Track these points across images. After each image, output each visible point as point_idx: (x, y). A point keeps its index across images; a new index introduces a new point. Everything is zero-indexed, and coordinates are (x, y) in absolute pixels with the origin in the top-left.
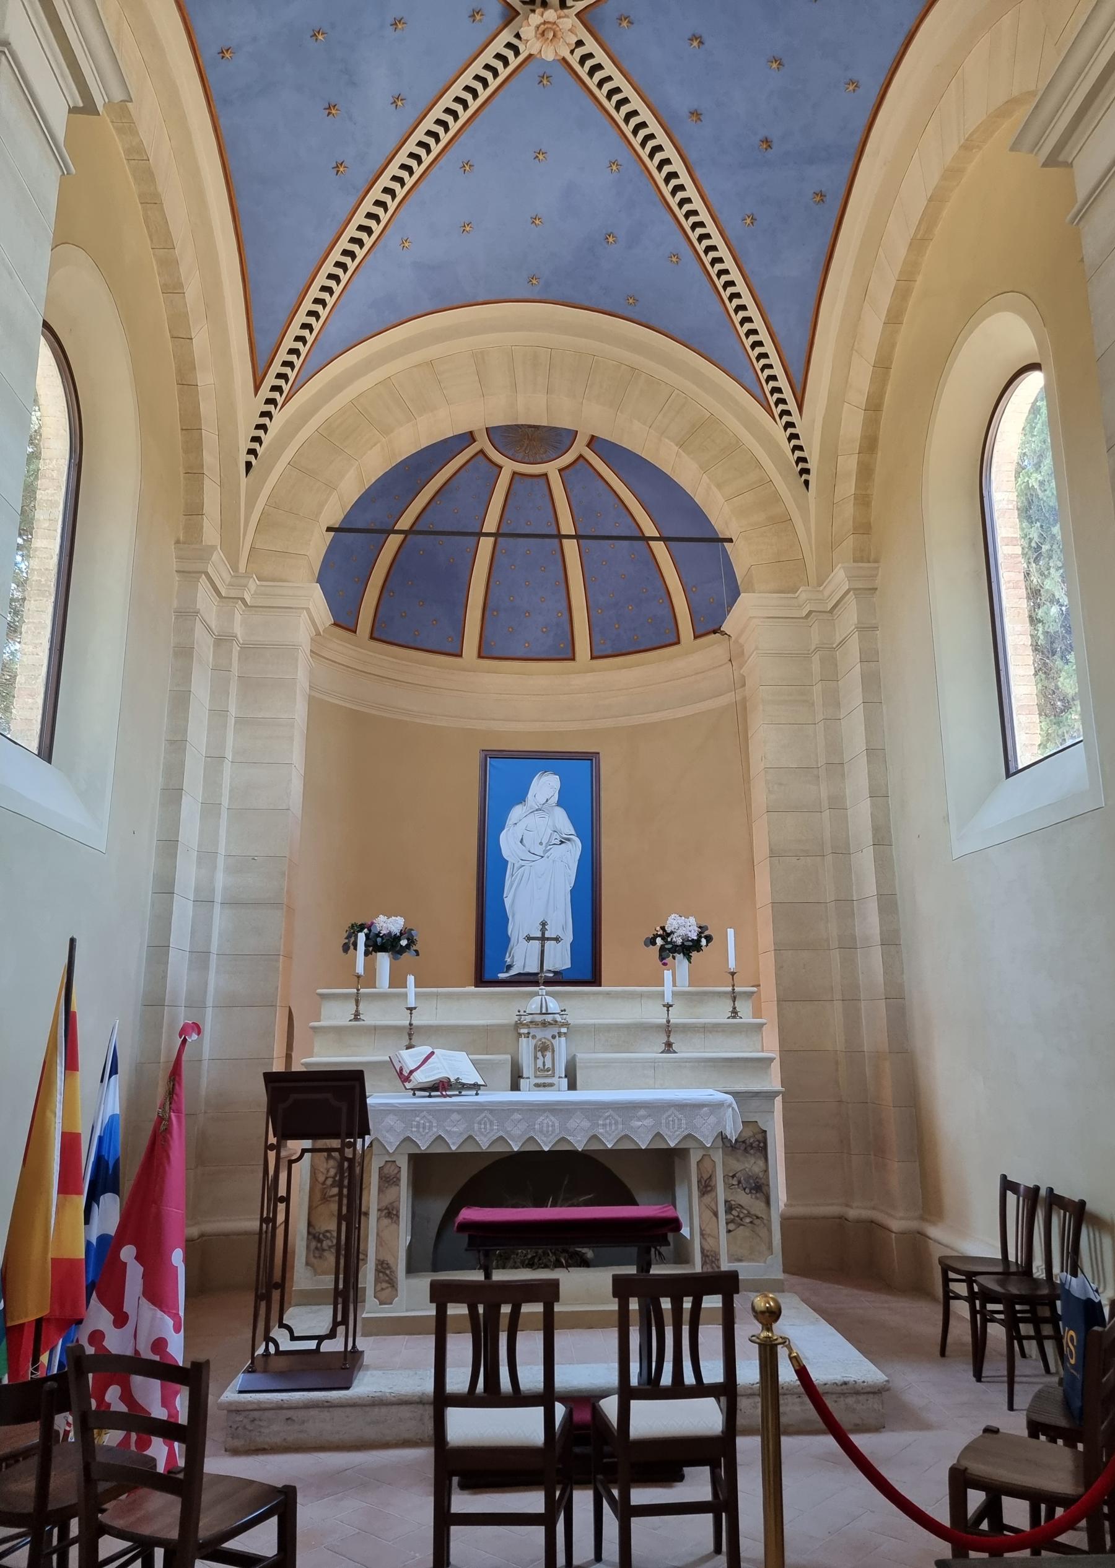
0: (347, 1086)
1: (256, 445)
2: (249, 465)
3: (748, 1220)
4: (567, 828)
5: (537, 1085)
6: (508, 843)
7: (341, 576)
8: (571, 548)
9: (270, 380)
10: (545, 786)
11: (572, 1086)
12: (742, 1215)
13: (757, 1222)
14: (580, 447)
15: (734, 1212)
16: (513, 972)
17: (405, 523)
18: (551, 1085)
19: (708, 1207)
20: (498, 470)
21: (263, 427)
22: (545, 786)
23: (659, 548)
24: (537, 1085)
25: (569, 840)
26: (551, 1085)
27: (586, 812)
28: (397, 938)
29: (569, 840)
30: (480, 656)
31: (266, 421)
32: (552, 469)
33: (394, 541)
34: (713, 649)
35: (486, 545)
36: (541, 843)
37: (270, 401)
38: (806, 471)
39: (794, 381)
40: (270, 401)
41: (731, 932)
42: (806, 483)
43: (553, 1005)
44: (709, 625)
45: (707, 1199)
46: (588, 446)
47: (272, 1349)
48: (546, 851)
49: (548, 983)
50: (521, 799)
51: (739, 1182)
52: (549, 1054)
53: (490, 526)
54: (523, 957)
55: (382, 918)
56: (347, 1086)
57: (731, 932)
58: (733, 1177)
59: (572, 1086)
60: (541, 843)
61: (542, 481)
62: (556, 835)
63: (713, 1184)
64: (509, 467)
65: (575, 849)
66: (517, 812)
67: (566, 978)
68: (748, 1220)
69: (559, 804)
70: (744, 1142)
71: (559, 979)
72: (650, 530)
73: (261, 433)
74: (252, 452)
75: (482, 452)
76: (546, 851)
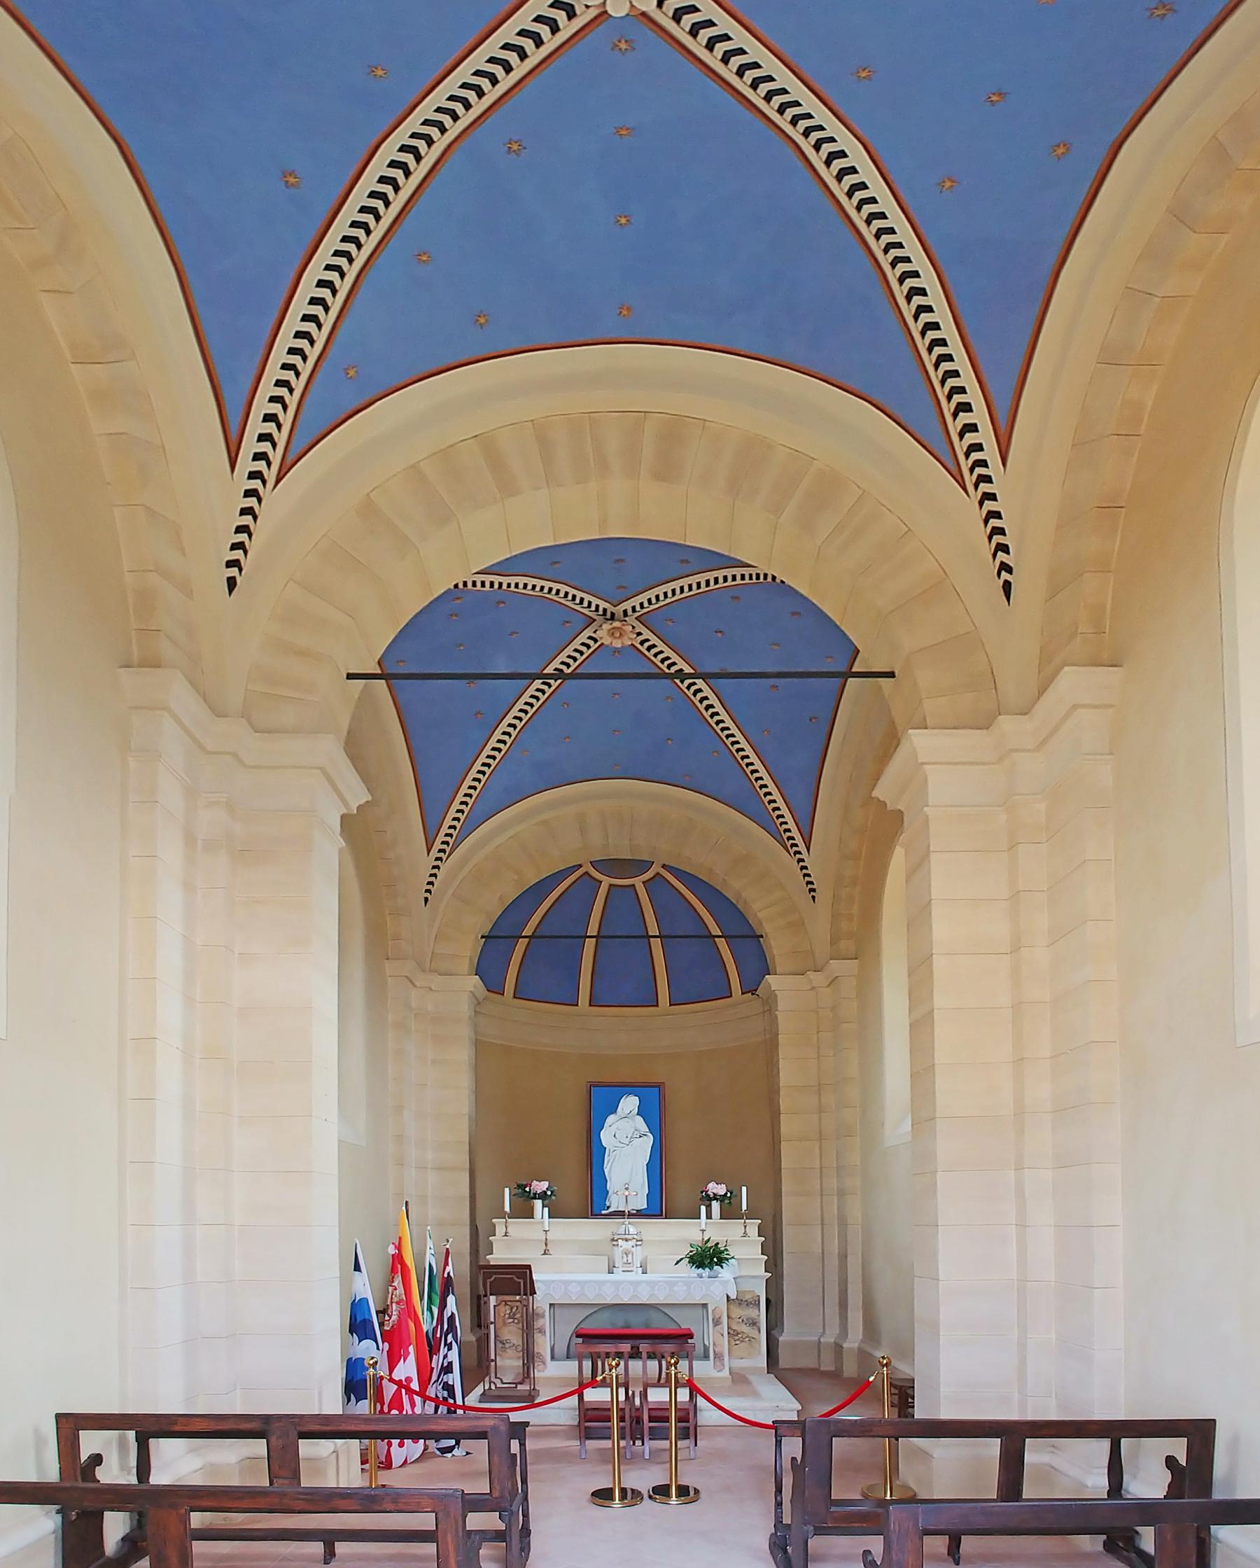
0: (524, 1272)
1: (430, 887)
2: (426, 899)
4: (643, 1127)
6: (606, 1137)
7: (489, 969)
8: (656, 944)
10: (629, 1103)
11: (644, 1272)
16: (611, 1210)
17: (528, 931)
21: (435, 875)
22: (629, 1103)
23: (721, 943)
27: (657, 1116)
28: (545, 1192)
31: (436, 871)
32: (638, 882)
33: (522, 943)
34: (750, 1005)
35: (590, 944)
37: (439, 859)
41: (744, 1189)
43: (632, 1230)
44: (751, 988)
47: (493, 1387)
49: (631, 1215)
50: (614, 1111)
53: (593, 930)
54: (615, 1203)
55: (535, 1183)
56: (524, 1272)
57: (744, 1189)
59: (644, 1272)
61: (632, 889)
64: (606, 881)
65: (650, 1140)
66: (611, 1119)
71: (639, 1214)
72: (716, 931)
73: (433, 879)
74: (428, 891)
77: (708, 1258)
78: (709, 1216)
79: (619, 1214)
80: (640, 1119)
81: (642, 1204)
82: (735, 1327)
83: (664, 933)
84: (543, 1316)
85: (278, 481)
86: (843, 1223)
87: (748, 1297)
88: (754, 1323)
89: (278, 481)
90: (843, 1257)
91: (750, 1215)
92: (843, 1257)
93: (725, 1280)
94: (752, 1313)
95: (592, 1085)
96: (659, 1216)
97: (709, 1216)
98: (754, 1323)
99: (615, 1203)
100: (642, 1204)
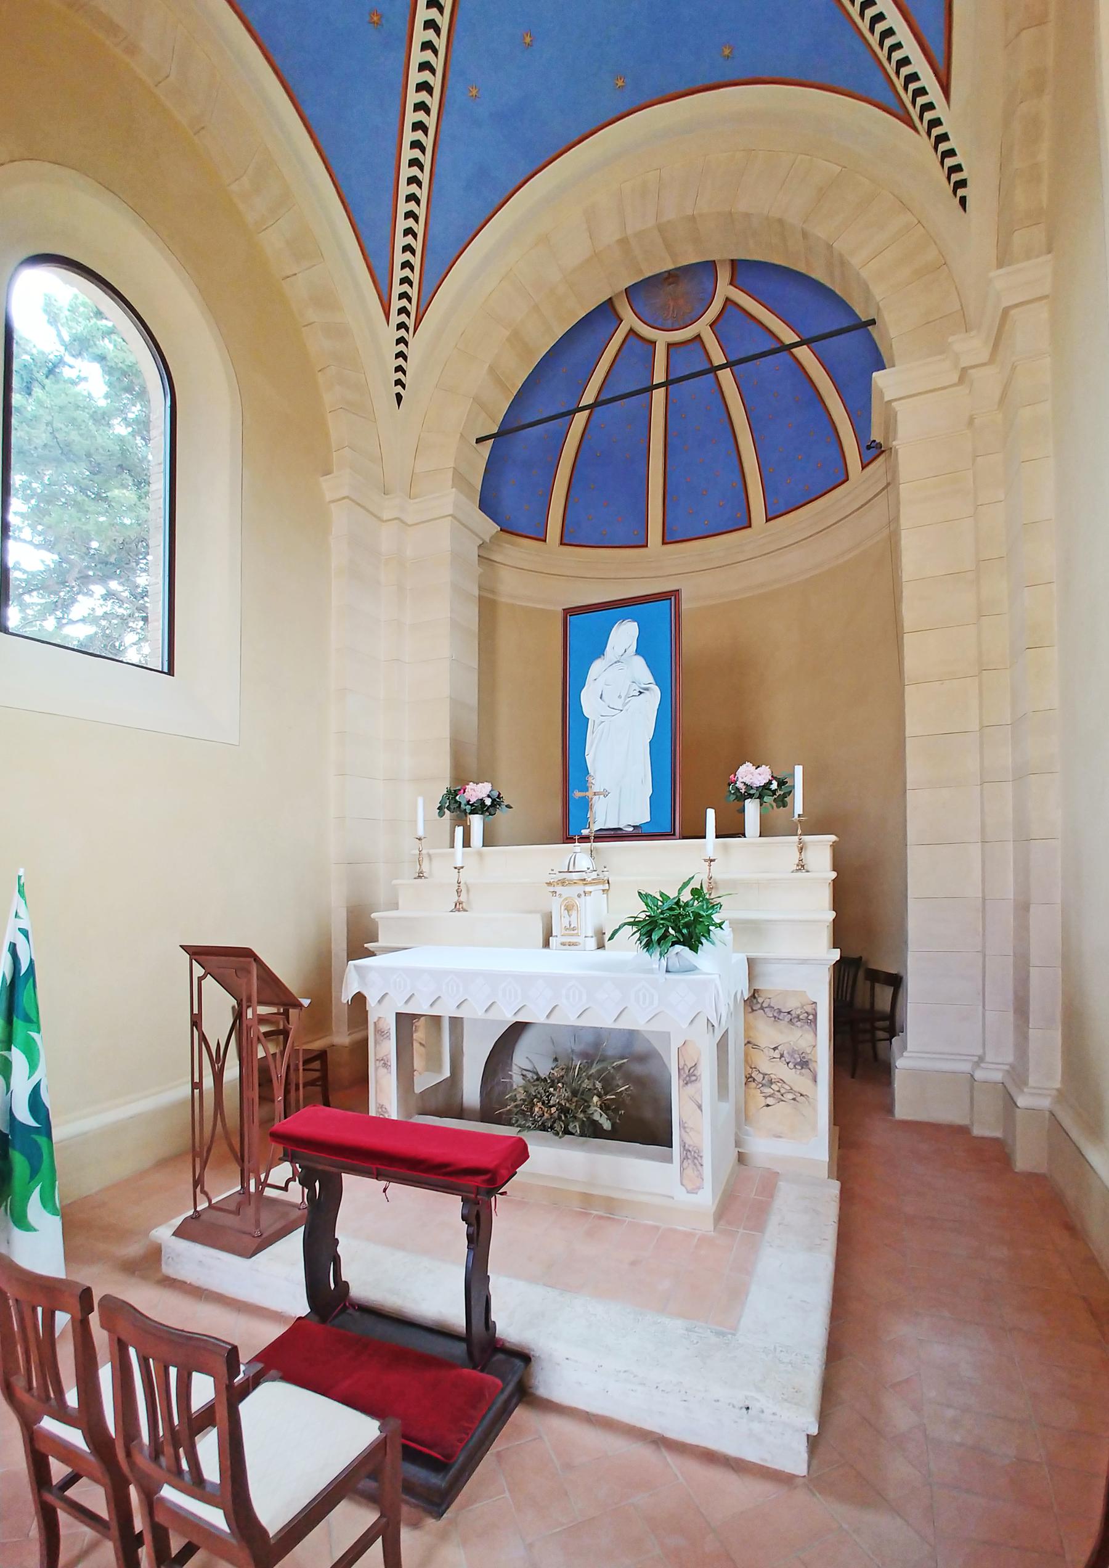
2: (399, 397)
3: (791, 1096)
5: (563, 944)
6: (589, 701)
9: (396, 304)
10: (624, 634)
12: (783, 1091)
13: (799, 1098)
14: (724, 289)
15: (773, 1086)
18: (574, 944)
19: (691, 1098)
20: (651, 347)
22: (624, 634)
23: (803, 353)
24: (563, 944)
25: (647, 689)
26: (574, 944)
27: (667, 656)
28: (482, 801)
29: (647, 689)
30: (664, 543)
36: (620, 697)
38: (962, 184)
39: (929, 43)
40: (401, 326)
42: (963, 201)
45: (690, 1088)
46: (731, 284)
48: (625, 704)
50: (600, 652)
51: (782, 1056)
52: (574, 913)
54: (603, 816)
58: (775, 1049)
60: (620, 697)
61: (696, 345)
62: (634, 686)
63: (697, 1073)
65: (654, 697)
66: (597, 667)
67: (645, 830)
68: (791, 1096)
69: (638, 652)
70: (789, 1013)
72: (788, 336)
75: (631, 331)
76: (625, 704)
77: (676, 926)
78: (467, 843)
79: (615, 835)
80: (640, 662)
81: (639, 813)
82: (765, 1066)
83: (732, 358)
84: (389, 1038)
85: (946, 89)
86: (1023, 838)
87: (792, 1004)
88: (804, 1063)
89: (946, 89)
90: (1023, 908)
91: (815, 825)
92: (1023, 908)
93: (717, 965)
94: (796, 1038)
95: (569, 612)
96: (669, 835)
97: (467, 843)
98: (804, 1063)
99: (603, 816)
100: (639, 813)
